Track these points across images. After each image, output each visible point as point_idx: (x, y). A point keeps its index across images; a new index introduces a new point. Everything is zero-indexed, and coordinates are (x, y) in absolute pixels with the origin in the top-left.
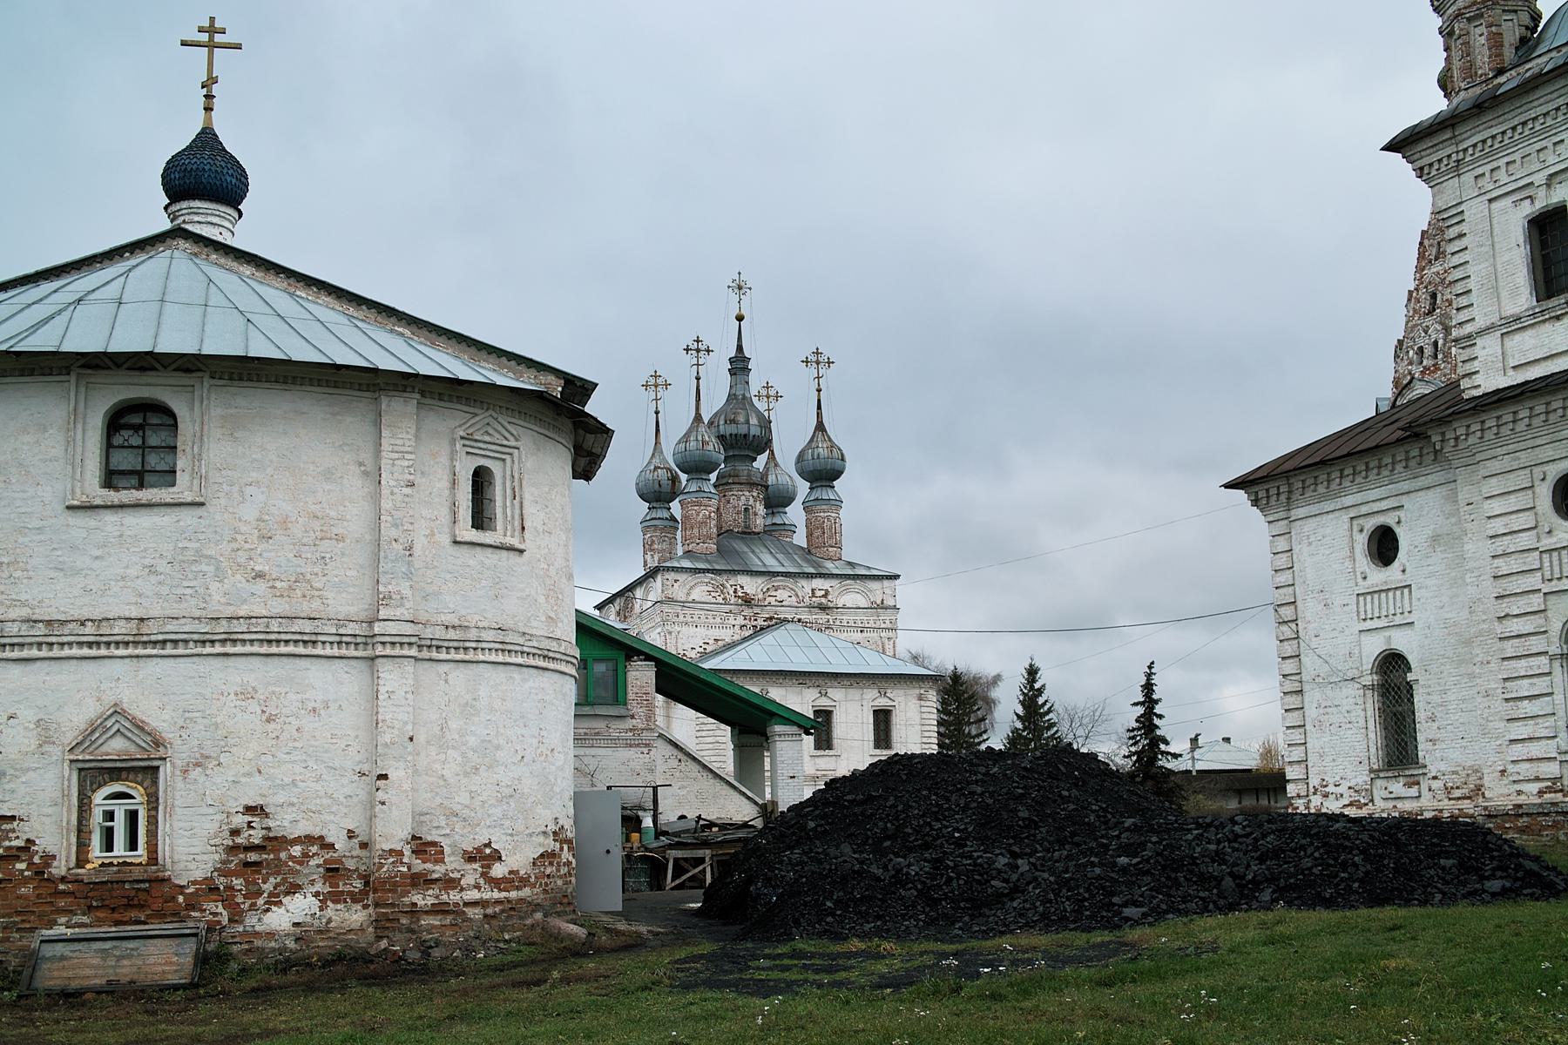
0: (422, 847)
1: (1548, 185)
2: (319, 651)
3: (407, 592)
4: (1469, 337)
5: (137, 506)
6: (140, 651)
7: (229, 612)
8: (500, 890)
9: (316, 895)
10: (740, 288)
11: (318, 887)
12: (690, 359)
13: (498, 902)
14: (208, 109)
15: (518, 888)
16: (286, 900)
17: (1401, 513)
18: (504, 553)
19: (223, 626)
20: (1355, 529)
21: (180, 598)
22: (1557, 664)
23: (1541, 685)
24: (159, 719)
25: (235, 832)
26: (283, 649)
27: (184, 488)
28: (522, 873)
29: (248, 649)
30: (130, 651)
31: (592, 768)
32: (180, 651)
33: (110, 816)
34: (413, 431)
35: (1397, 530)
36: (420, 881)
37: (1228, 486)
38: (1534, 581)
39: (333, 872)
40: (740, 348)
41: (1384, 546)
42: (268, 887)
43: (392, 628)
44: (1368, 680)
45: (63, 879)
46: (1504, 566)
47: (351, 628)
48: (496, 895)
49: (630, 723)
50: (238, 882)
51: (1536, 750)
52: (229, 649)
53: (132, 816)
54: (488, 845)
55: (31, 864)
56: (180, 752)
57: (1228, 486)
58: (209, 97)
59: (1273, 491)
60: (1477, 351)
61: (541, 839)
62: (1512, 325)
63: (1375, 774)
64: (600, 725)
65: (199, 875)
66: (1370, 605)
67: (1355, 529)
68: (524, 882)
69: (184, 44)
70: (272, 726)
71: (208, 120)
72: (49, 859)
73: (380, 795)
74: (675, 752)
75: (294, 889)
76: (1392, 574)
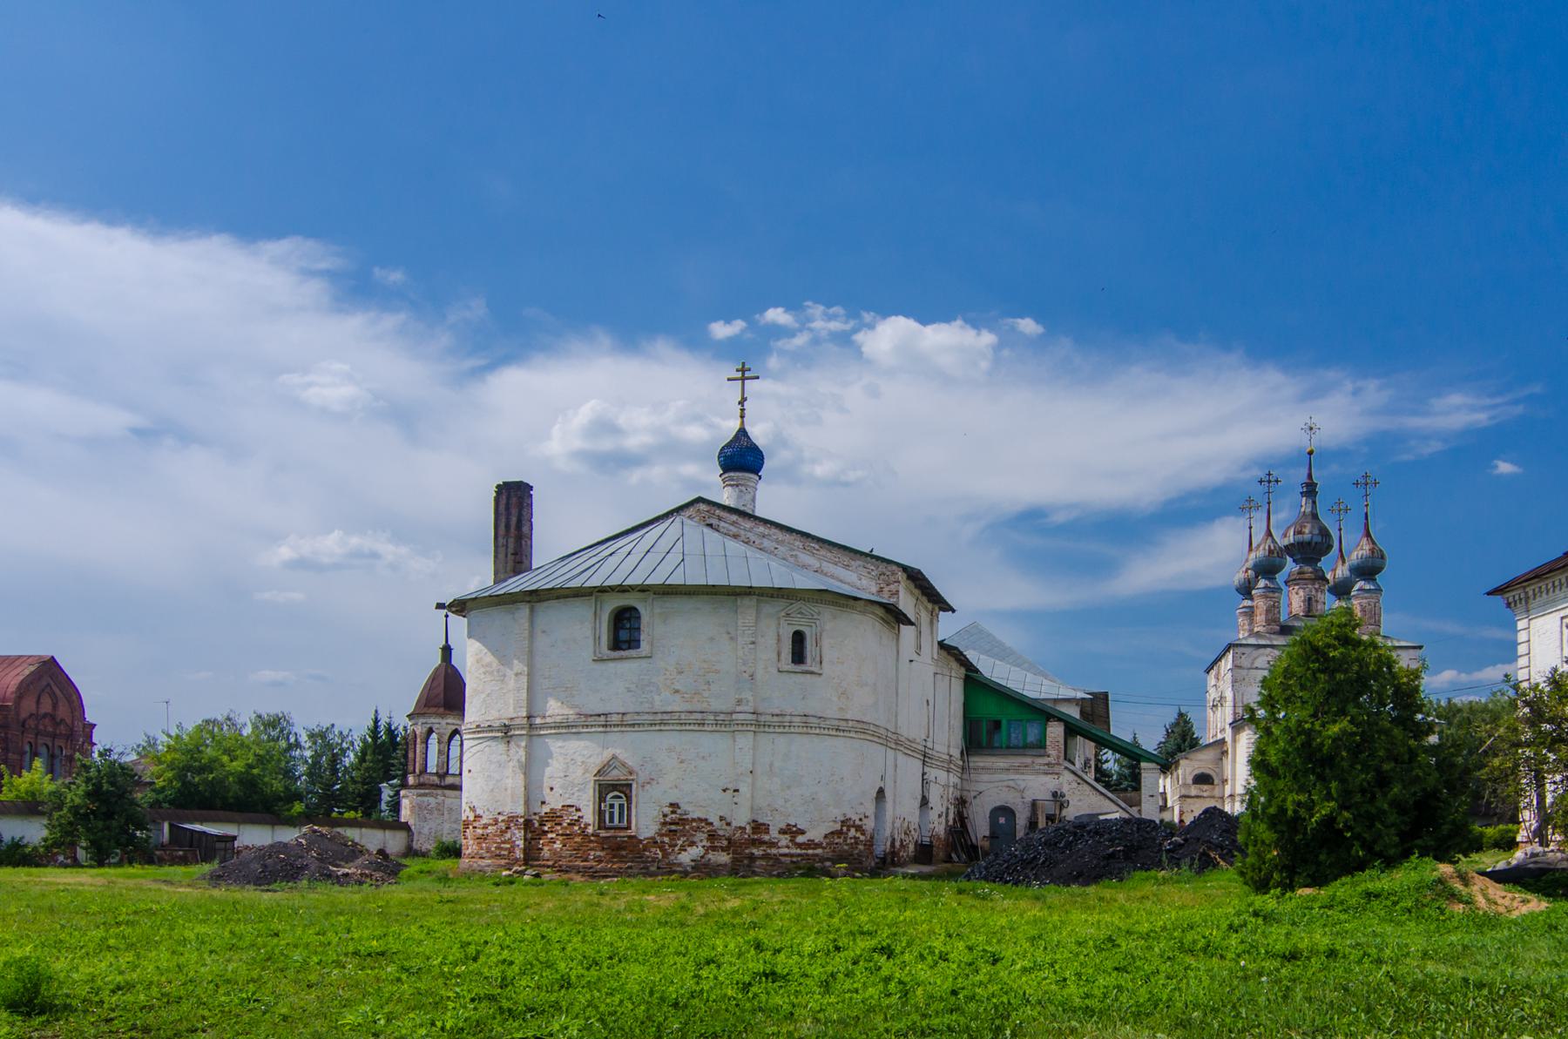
0: (759, 827)
2: (706, 728)
3: (751, 698)
6: (623, 729)
7: (663, 710)
8: (801, 849)
9: (703, 847)
10: (1311, 429)
11: (705, 843)
12: (1263, 488)
13: (799, 855)
14: (742, 417)
15: (814, 849)
16: (689, 849)
18: (808, 676)
19: (659, 717)
21: (641, 703)
25: (665, 816)
26: (688, 727)
27: (645, 647)
28: (816, 841)
29: (671, 727)
30: (619, 729)
31: (1022, 787)
33: (612, 806)
34: (754, 614)
37: (1489, 594)
39: (712, 836)
40: (1310, 476)
42: (680, 842)
43: (741, 716)
45: (593, 835)
48: (799, 851)
49: (1046, 760)
50: (666, 839)
52: (662, 728)
53: (621, 806)
54: (795, 826)
55: (580, 828)
56: (642, 778)
57: (1489, 594)
58: (743, 410)
61: (831, 824)
64: (1028, 760)
68: (818, 845)
69: (729, 380)
71: (743, 423)
74: (1076, 778)
75: (692, 844)
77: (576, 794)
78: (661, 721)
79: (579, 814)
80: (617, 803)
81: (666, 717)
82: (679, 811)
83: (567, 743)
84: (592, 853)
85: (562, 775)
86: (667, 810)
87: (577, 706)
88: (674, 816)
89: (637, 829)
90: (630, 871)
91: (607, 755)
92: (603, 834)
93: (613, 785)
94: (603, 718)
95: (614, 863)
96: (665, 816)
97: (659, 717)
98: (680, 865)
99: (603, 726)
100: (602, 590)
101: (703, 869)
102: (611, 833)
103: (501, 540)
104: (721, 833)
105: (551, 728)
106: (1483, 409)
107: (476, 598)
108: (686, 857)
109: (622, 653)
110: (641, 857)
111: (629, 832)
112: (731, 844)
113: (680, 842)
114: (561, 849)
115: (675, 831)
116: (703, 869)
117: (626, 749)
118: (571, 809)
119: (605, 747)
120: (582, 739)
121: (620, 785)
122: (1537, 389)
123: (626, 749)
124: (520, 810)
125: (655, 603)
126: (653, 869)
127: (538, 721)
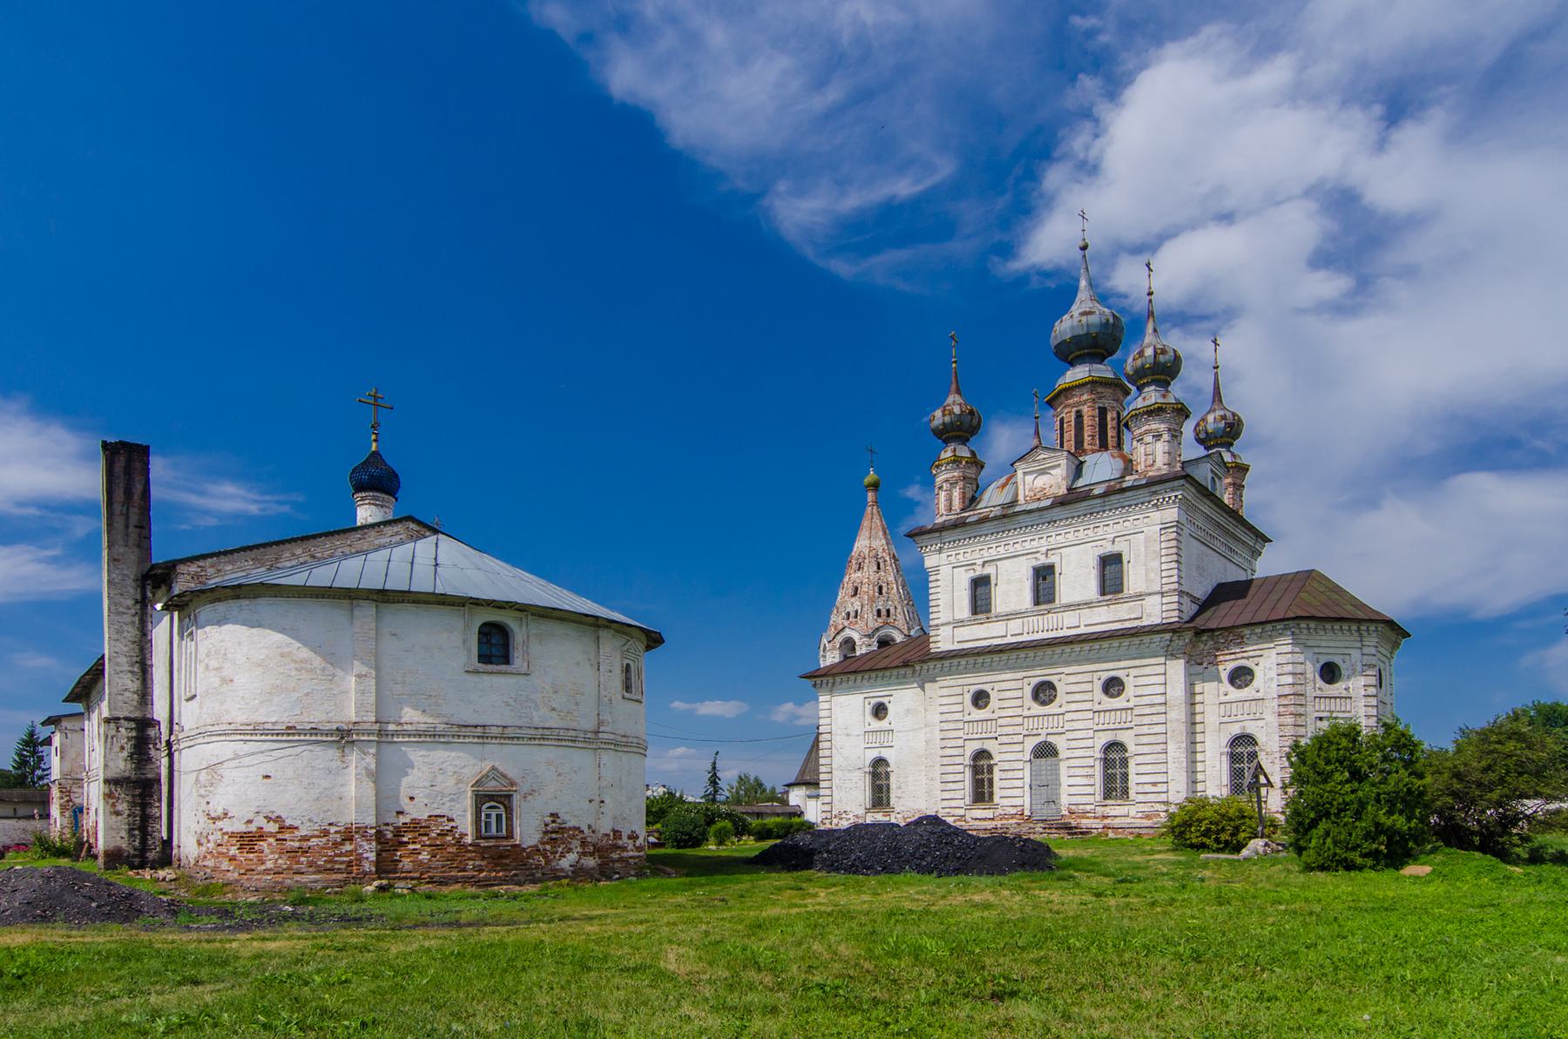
0: (617, 834)
1: (983, 566)
4: (937, 626)
5: (499, 673)
6: (502, 741)
7: (541, 725)
13: (638, 857)
17: (891, 698)
19: (541, 732)
20: (867, 703)
22: (967, 769)
23: (959, 777)
24: (512, 773)
25: (546, 825)
26: (563, 743)
27: (518, 662)
29: (550, 742)
30: (498, 741)
32: (520, 742)
33: (488, 816)
35: (888, 705)
36: (616, 847)
38: (960, 733)
41: (880, 711)
42: (560, 850)
44: (867, 770)
45: (470, 845)
46: (945, 726)
47: (589, 735)
50: (548, 847)
51: (953, 803)
53: (499, 817)
59: (825, 682)
60: (939, 632)
62: (959, 624)
63: (868, 811)
65: (532, 844)
66: (871, 737)
67: (867, 703)
70: (560, 778)
72: (463, 835)
73: (602, 810)
75: (570, 850)
76: (884, 724)
77: (448, 804)
78: (542, 736)
79: (452, 824)
80: (494, 813)
81: (546, 732)
82: (558, 821)
83: (432, 753)
84: (471, 863)
85: (428, 784)
86: (548, 819)
87: (444, 716)
88: (554, 825)
89: (521, 837)
90: (516, 878)
91: (487, 766)
92: (483, 843)
93: (488, 796)
94: (479, 729)
95: (497, 872)
96: (546, 825)
97: (541, 732)
98: (562, 870)
99: (478, 737)
100: (476, 603)
101: (579, 874)
102: (492, 843)
103: (117, 508)
104: (589, 840)
105: (409, 736)
106: (255, 502)
107: (239, 586)
108: (566, 862)
109: (490, 667)
110: (525, 865)
111: (511, 842)
112: (598, 850)
113: (560, 850)
114: (430, 860)
115: (555, 839)
116: (579, 874)
117: (507, 760)
118: (440, 820)
119: (483, 759)
120: (452, 750)
121: (500, 796)
122: (301, 498)
123: (507, 760)
124: (370, 820)
125: (356, 612)
126: (539, 875)
127: (391, 727)
